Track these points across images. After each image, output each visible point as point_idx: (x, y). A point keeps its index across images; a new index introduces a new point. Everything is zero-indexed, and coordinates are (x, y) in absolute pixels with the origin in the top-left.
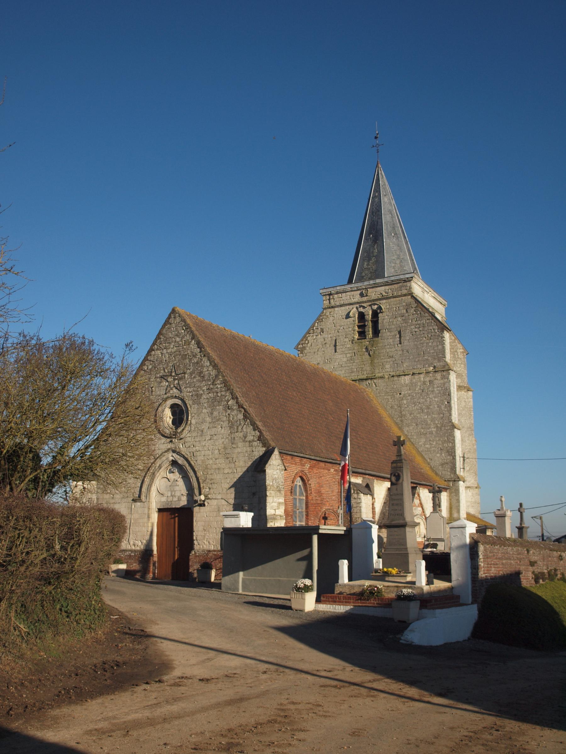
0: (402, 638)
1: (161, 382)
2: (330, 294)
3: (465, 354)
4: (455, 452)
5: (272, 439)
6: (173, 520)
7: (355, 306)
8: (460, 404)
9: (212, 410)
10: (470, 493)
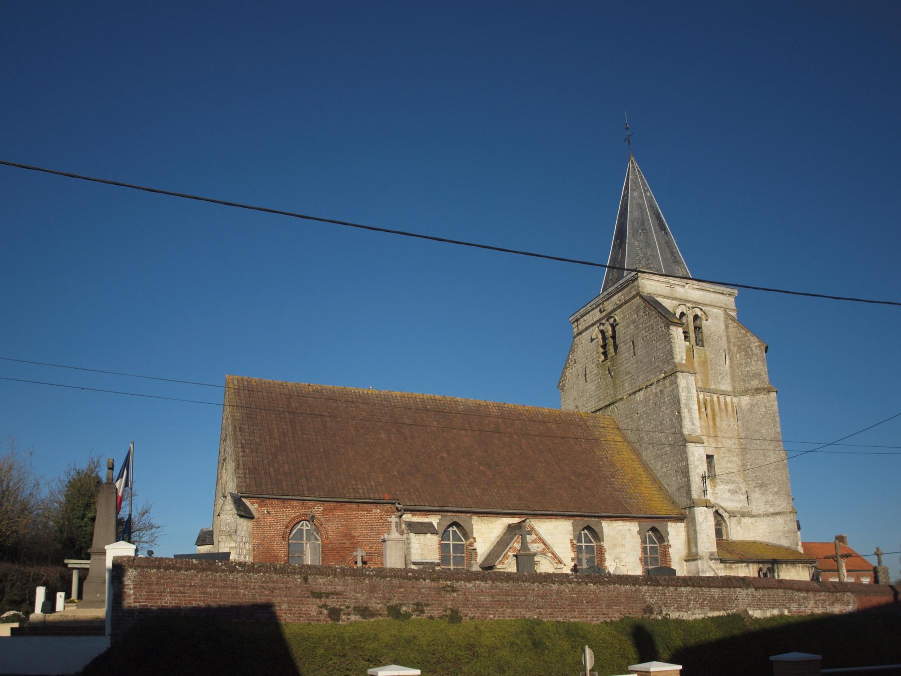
2: (577, 320)
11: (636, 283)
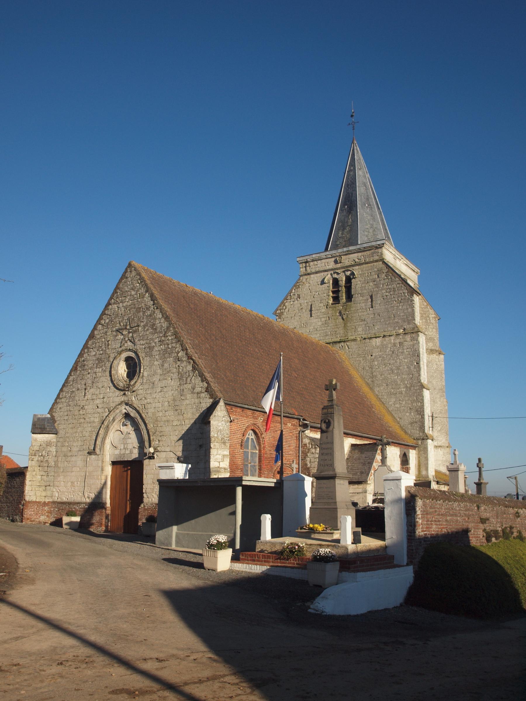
0: (311, 606)
1: (116, 336)
3: (437, 319)
4: (423, 411)
5: (220, 390)
6: (125, 473)
7: (329, 273)
8: (431, 367)
9: (163, 361)
10: (440, 452)
11: (380, 250)
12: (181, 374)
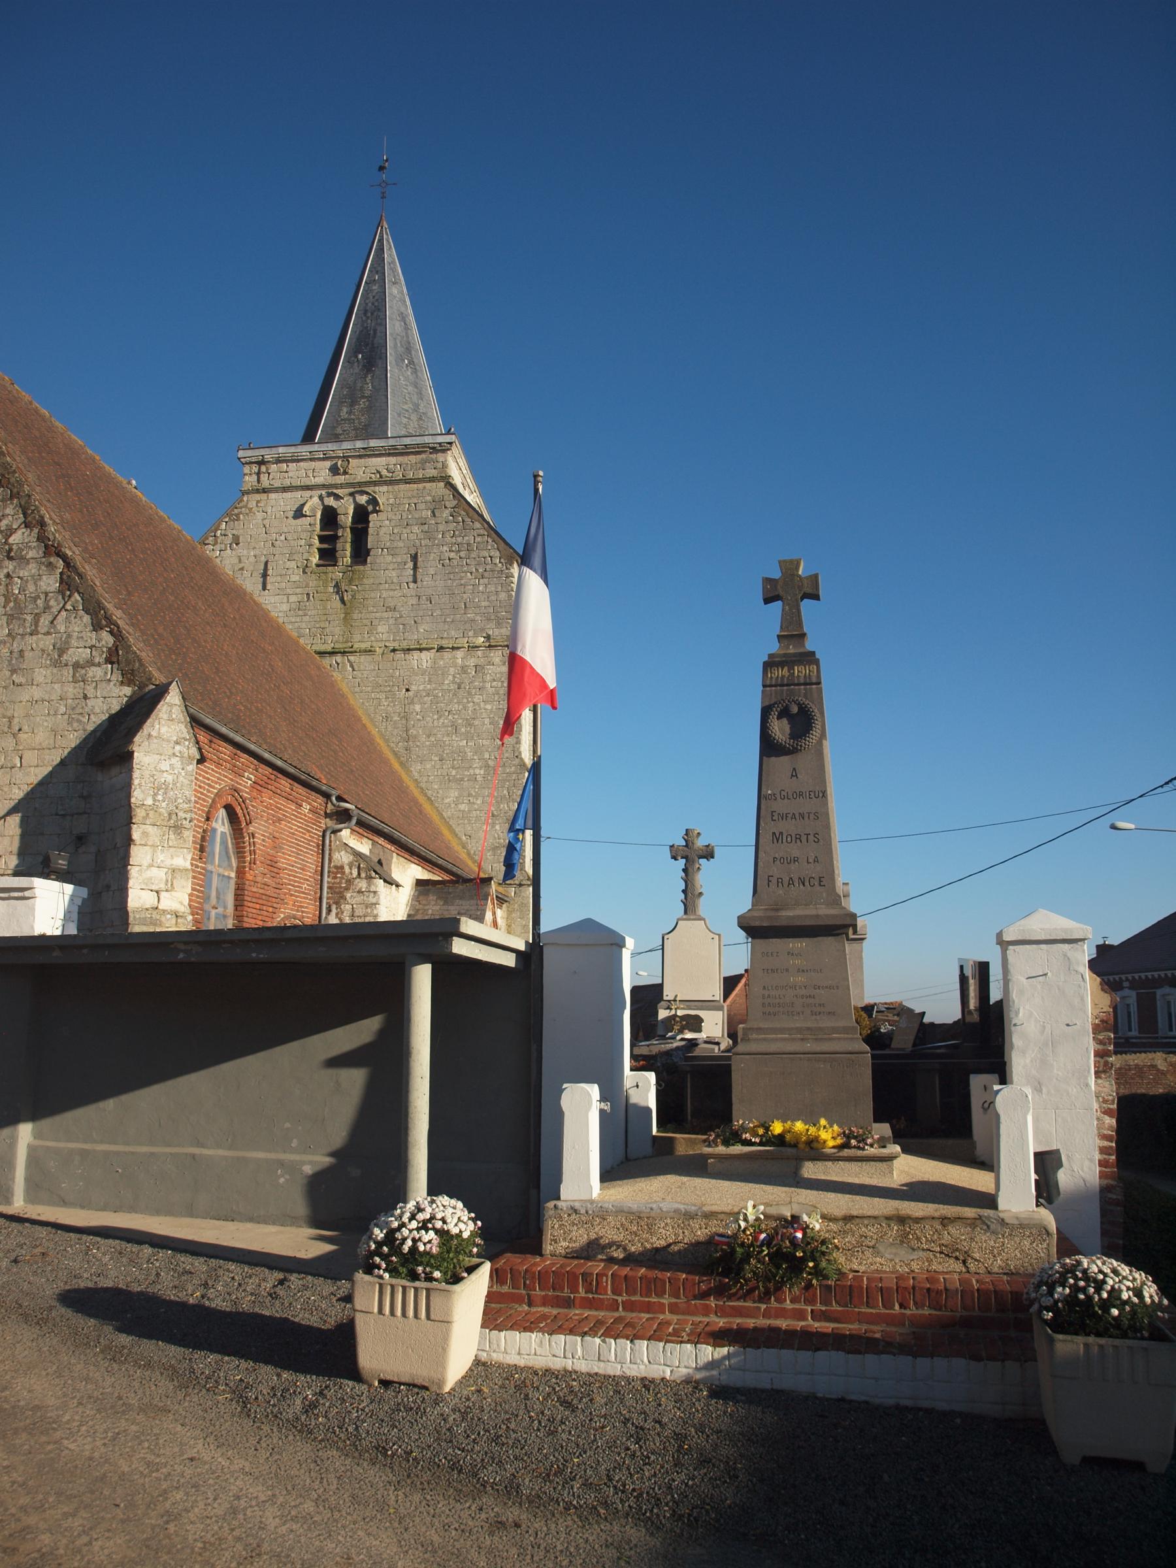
2: (261, 463)
7: (317, 493)
11: (440, 457)
12: (16, 600)
